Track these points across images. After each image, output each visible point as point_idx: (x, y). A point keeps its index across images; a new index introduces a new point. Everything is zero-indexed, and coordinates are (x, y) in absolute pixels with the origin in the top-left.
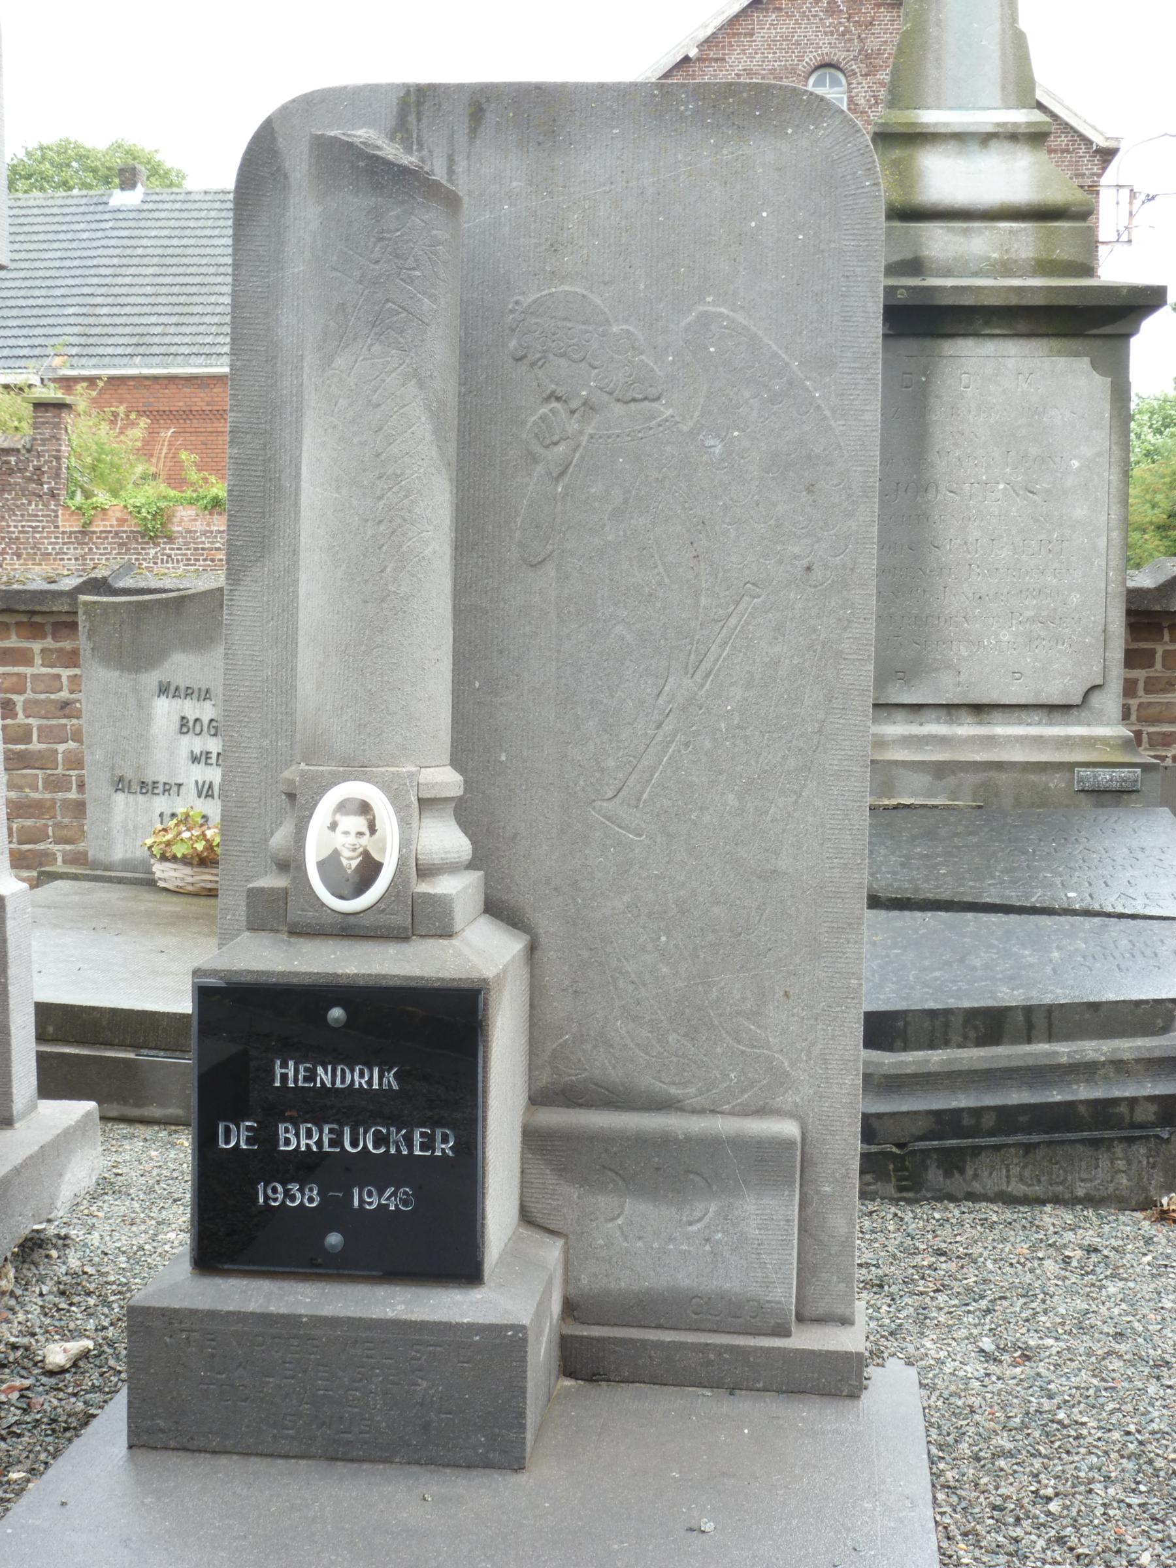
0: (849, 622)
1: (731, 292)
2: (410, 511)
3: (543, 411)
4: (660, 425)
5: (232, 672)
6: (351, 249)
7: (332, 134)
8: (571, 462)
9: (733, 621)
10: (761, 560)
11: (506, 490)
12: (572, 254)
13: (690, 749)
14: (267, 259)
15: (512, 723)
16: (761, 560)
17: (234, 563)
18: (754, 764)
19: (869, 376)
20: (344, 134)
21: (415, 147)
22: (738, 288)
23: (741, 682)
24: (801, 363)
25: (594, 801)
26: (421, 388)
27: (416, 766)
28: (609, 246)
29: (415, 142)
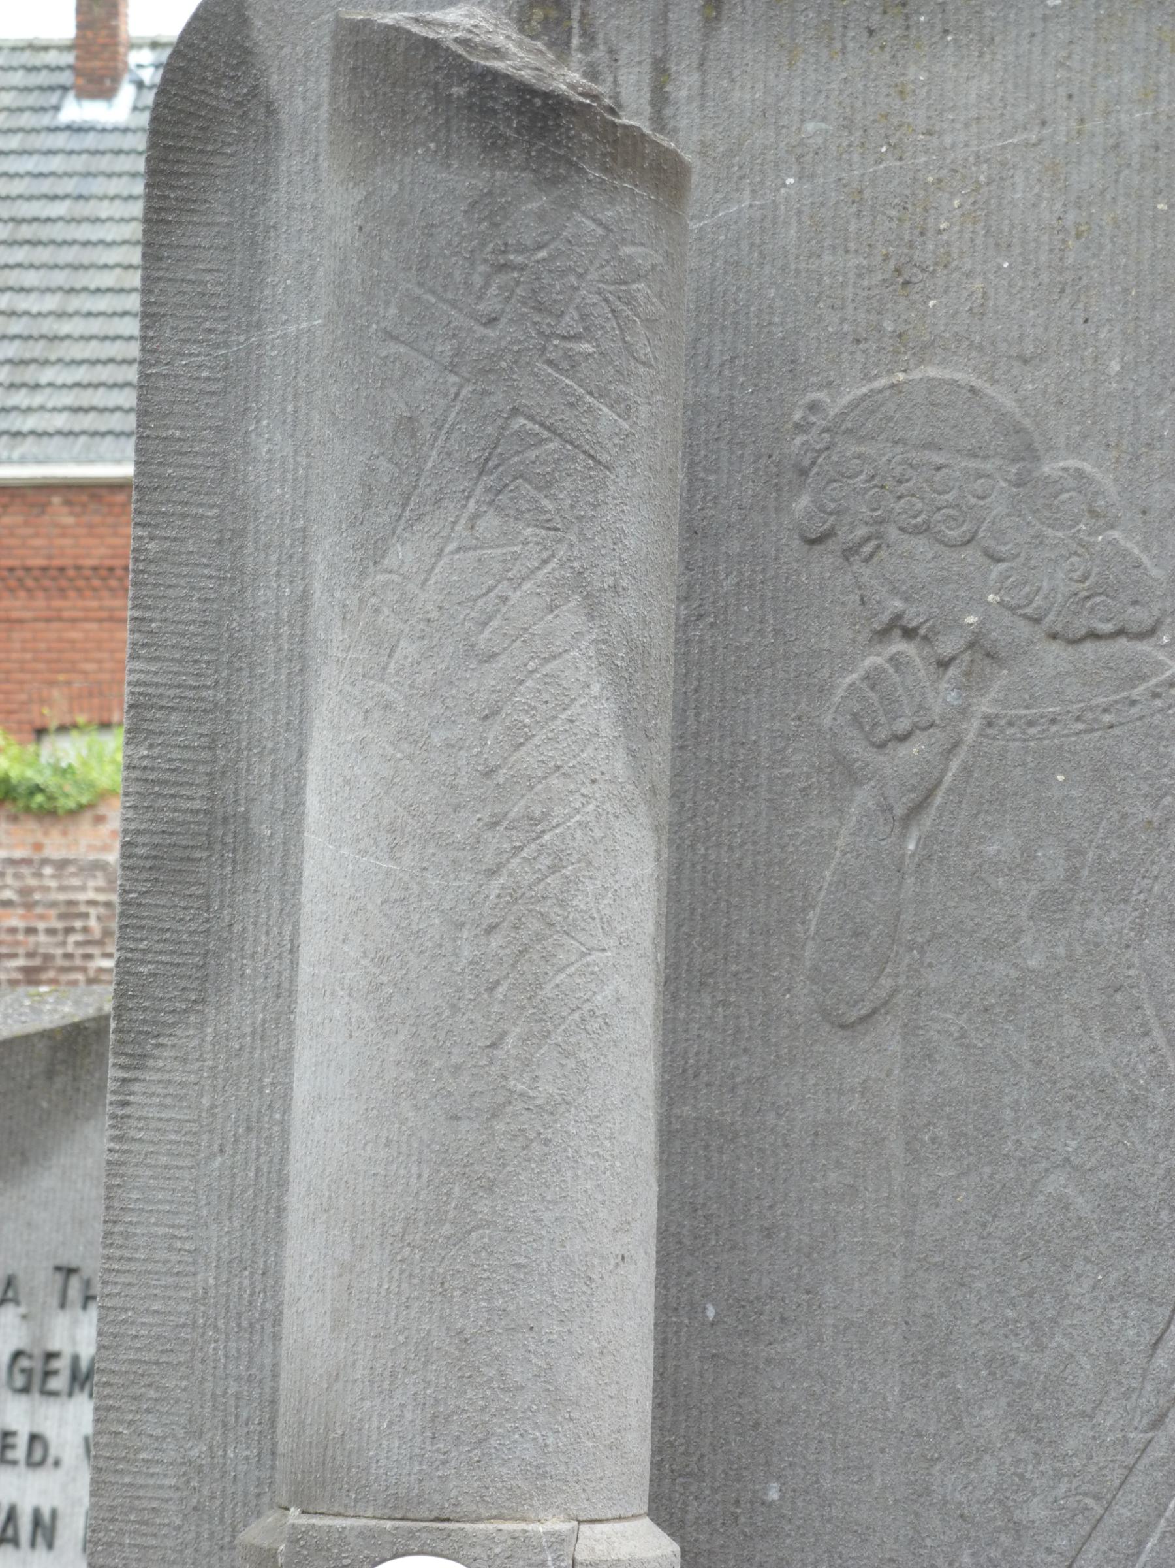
2: (562, 903)
3: (871, 661)
4: (1156, 695)
5: (121, 1279)
6: (433, 292)
7: (390, 18)
8: (939, 782)
11: (783, 848)
12: (946, 292)
14: (222, 302)
17: (134, 1016)
20: (417, 20)
21: (575, 41)
26: (591, 616)
27: (570, 1518)
28: (1035, 274)
29: (576, 30)
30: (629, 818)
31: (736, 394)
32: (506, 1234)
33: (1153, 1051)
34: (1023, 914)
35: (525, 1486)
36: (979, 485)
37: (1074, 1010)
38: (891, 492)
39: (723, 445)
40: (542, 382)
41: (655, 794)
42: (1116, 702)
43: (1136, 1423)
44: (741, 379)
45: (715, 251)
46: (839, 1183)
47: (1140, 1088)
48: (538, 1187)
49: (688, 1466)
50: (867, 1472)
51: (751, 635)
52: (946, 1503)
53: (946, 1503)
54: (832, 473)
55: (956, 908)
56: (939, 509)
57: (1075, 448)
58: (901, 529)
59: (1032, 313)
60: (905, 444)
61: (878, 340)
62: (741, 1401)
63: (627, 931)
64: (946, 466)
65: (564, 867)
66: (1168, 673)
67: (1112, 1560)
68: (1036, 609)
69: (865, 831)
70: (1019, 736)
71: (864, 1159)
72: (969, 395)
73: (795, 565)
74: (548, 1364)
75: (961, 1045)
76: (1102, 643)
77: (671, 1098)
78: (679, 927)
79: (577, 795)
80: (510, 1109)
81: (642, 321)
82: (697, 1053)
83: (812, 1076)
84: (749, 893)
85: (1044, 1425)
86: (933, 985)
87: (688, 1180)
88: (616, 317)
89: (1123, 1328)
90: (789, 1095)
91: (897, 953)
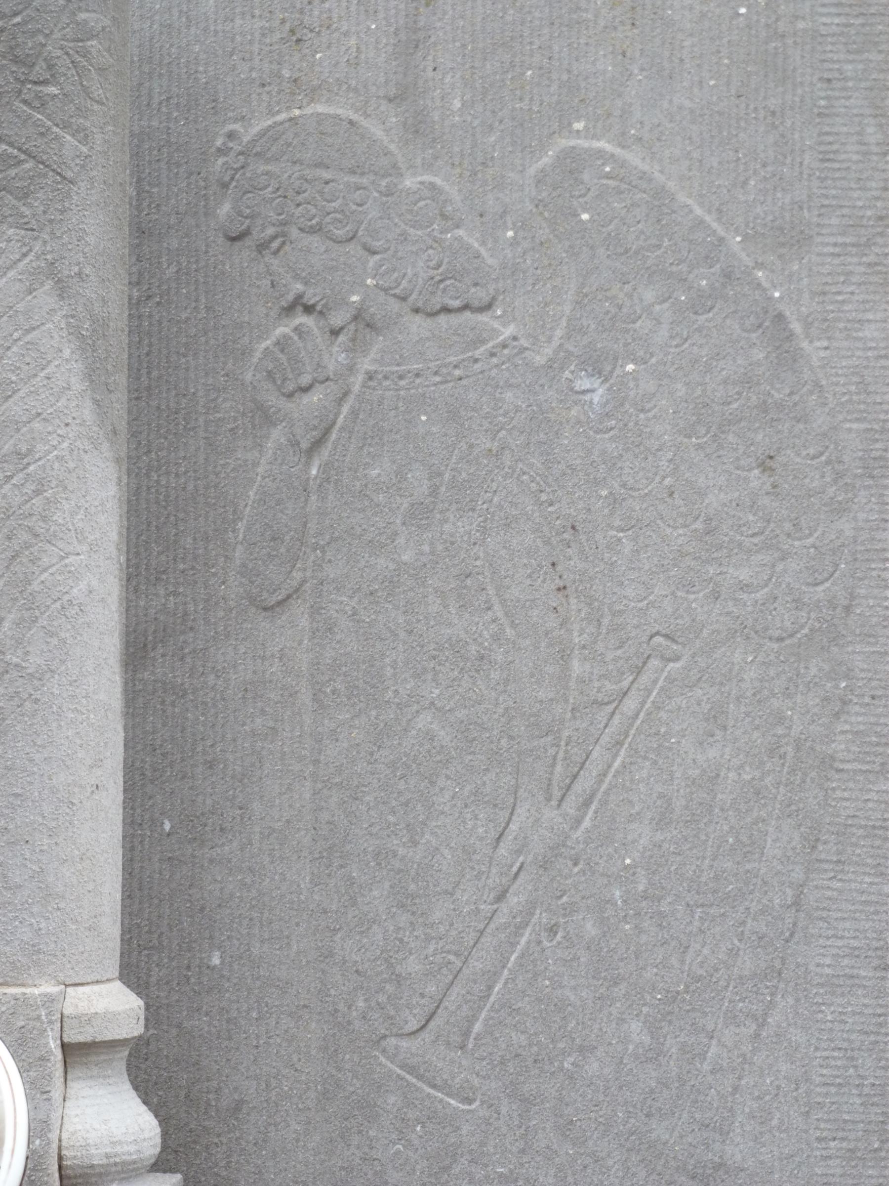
0: (844, 703)
1: (617, 113)
2: (44, 519)
3: (280, 330)
4: (493, 355)
9: (630, 704)
10: (679, 594)
12: (329, 47)
13: (559, 937)
15: (232, 895)
16: (679, 594)
18: (677, 965)
19: (872, 258)
22: (631, 105)
23: (649, 815)
24: (745, 238)
25: (384, 1037)
26: (61, 297)
30: (96, 453)
31: (171, 125)
32: (6, 771)
33: (494, 621)
34: (398, 521)
35: (24, 960)
36: (358, 195)
37: (436, 592)
38: (292, 201)
39: (163, 165)
40: (19, 117)
41: (115, 433)
42: (463, 360)
43: (485, 898)
44: (175, 114)
45: (152, 16)
46: (263, 726)
47: (485, 649)
48: (30, 735)
49: (150, 941)
50: (286, 941)
51: (188, 311)
52: (345, 962)
53: (345, 962)
54: (247, 186)
55: (348, 517)
56: (328, 214)
57: (428, 167)
58: (301, 229)
59: (394, 63)
60: (302, 164)
61: (279, 84)
62: (191, 892)
63: (96, 540)
64: (333, 181)
65: (45, 491)
66: (501, 338)
67: (469, 1001)
68: (403, 290)
69: (279, 461)
70: (392, 387)
71: (282, 708)
72: (348, 126)
73: (221, 257)
74: (40, 868)
75: (353, 620)
76: (452, 315)
77: (135, 666)
78: (139, 536)
79: (55, 436)
80: (7, 677)
81: (95, 70)
82: (155, 631)
83: (242, 646)
84: (192, 509)
85: (417, 901)
86: (332, 576)
87: (149, 728)
88: (75, 67)
89: (474, 827)
90: (225, 661)
91: (305, 552)
